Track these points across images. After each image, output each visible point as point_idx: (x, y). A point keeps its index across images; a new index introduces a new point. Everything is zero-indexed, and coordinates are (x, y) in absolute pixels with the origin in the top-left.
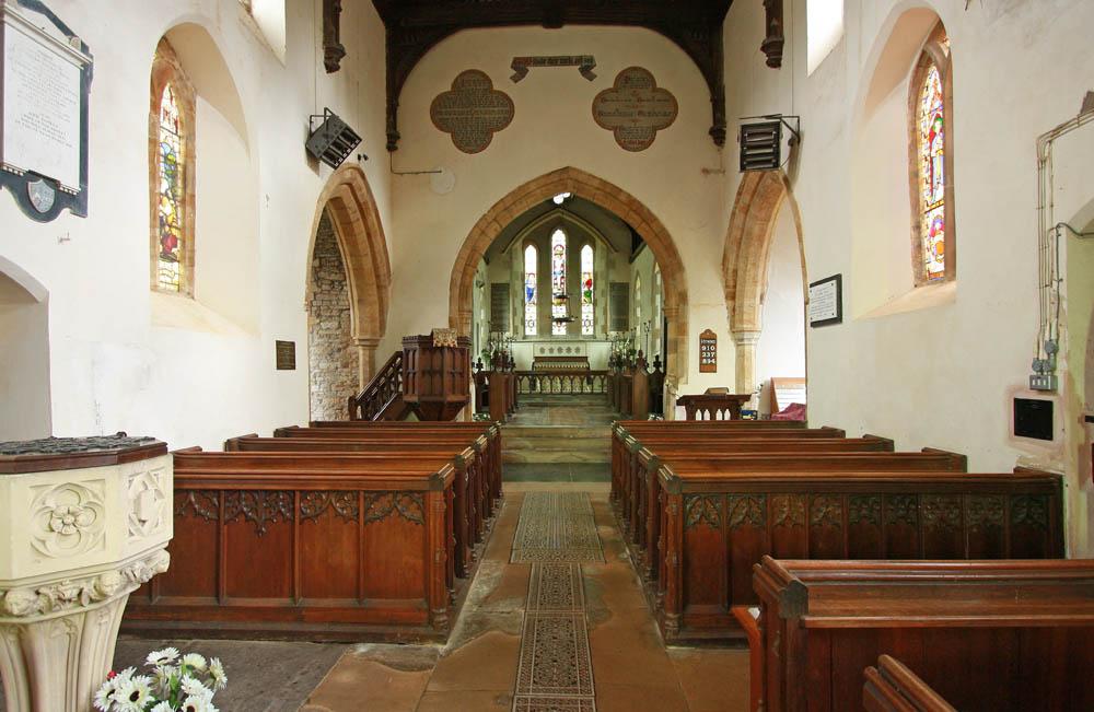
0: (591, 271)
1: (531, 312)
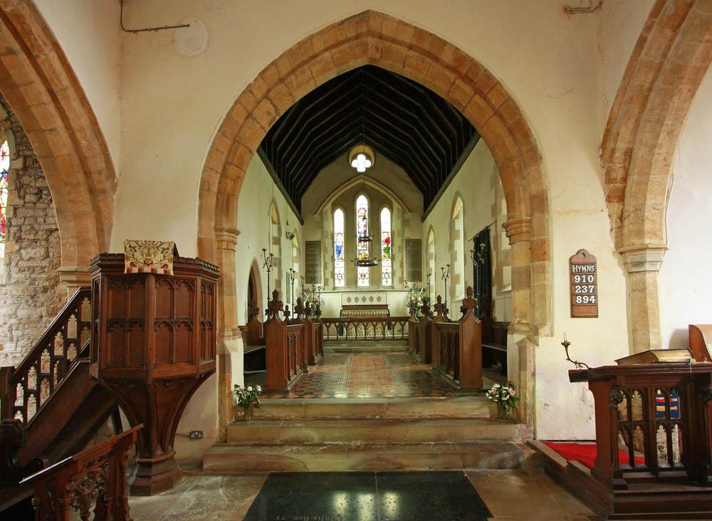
0: (389, 231)
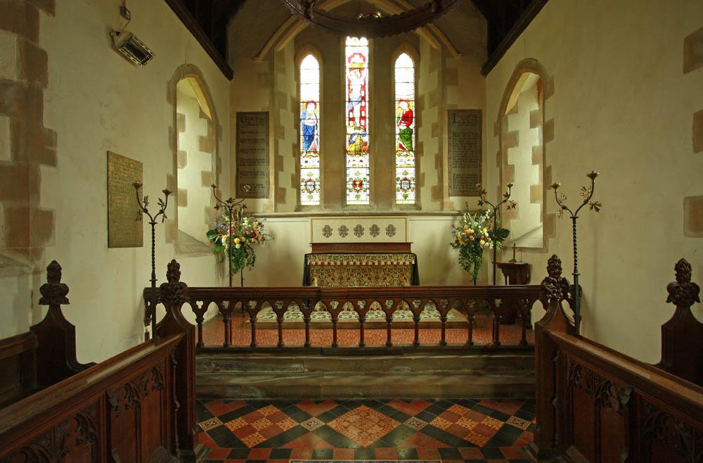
1: (311, 167)
